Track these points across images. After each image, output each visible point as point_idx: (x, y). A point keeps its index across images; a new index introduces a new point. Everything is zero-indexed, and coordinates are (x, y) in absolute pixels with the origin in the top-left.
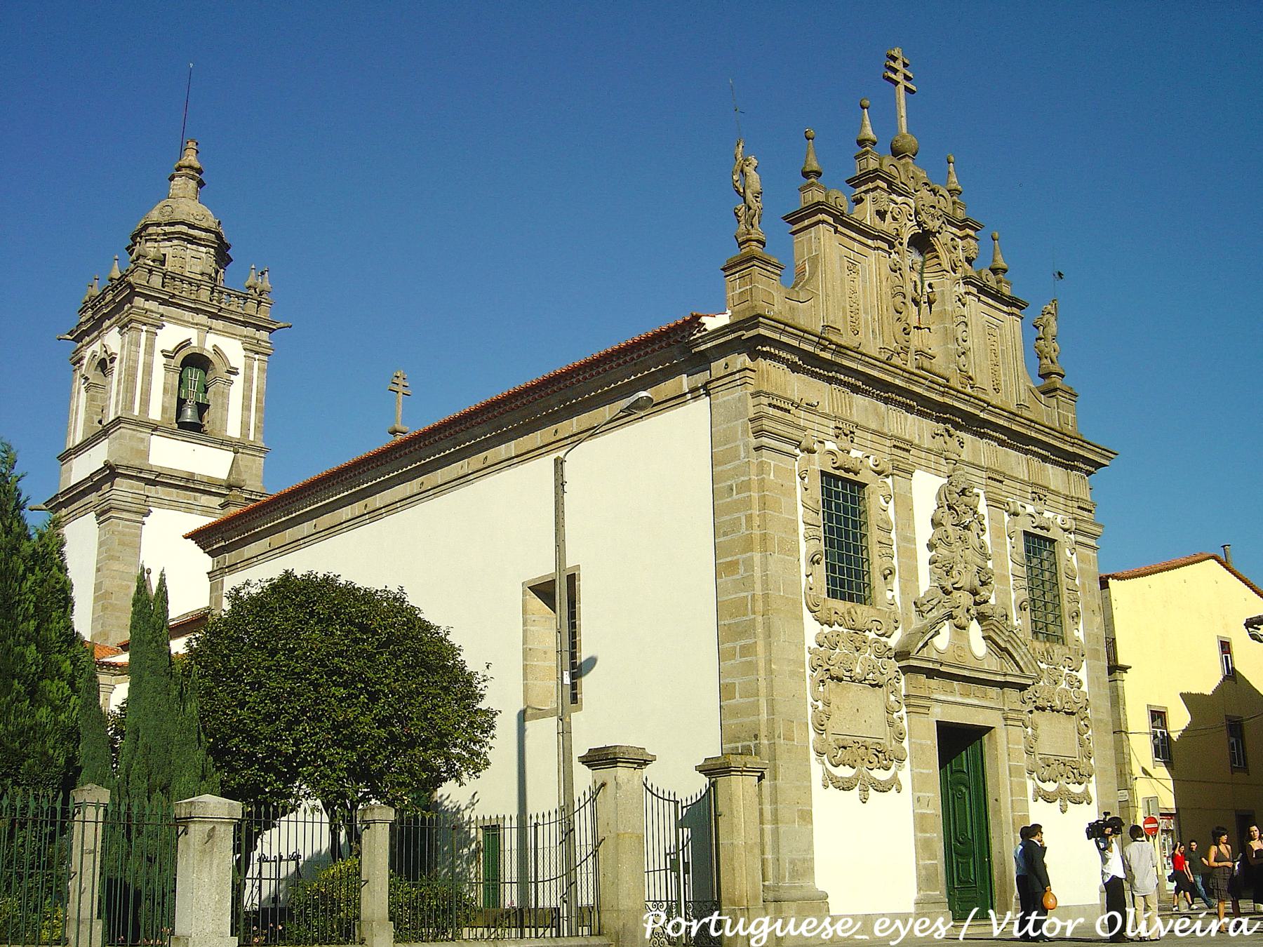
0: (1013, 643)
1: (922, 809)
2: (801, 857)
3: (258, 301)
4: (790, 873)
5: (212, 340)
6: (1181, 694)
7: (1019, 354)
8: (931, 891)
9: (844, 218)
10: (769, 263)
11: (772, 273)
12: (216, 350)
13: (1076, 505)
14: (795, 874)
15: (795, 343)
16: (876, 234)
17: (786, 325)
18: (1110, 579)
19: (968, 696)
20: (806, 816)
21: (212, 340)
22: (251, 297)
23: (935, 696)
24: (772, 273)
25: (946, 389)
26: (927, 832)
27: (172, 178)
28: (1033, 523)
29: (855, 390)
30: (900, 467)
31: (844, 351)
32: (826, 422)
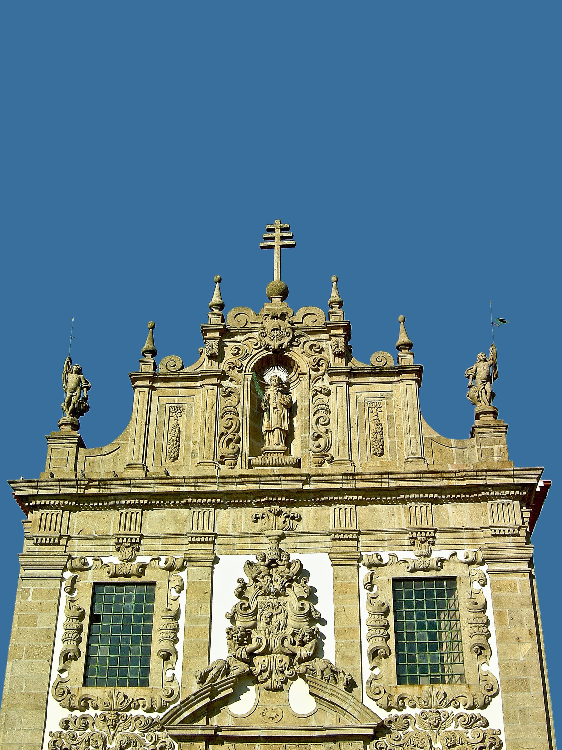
0: (337, 695)
6: (249, 690)
7: (411, 413)
9: (159, 376)
10: (63, 438)
11: (67, 443)
13: (489, 534)
15: (56, 491)
16: (200, 375)
18: (305, 597)
24: (67, 443)
25: (243, 479)
28: (408, 568)
29: (217, 506)
30: (192, 559)
31: (109, 482)
32: (105, 542)
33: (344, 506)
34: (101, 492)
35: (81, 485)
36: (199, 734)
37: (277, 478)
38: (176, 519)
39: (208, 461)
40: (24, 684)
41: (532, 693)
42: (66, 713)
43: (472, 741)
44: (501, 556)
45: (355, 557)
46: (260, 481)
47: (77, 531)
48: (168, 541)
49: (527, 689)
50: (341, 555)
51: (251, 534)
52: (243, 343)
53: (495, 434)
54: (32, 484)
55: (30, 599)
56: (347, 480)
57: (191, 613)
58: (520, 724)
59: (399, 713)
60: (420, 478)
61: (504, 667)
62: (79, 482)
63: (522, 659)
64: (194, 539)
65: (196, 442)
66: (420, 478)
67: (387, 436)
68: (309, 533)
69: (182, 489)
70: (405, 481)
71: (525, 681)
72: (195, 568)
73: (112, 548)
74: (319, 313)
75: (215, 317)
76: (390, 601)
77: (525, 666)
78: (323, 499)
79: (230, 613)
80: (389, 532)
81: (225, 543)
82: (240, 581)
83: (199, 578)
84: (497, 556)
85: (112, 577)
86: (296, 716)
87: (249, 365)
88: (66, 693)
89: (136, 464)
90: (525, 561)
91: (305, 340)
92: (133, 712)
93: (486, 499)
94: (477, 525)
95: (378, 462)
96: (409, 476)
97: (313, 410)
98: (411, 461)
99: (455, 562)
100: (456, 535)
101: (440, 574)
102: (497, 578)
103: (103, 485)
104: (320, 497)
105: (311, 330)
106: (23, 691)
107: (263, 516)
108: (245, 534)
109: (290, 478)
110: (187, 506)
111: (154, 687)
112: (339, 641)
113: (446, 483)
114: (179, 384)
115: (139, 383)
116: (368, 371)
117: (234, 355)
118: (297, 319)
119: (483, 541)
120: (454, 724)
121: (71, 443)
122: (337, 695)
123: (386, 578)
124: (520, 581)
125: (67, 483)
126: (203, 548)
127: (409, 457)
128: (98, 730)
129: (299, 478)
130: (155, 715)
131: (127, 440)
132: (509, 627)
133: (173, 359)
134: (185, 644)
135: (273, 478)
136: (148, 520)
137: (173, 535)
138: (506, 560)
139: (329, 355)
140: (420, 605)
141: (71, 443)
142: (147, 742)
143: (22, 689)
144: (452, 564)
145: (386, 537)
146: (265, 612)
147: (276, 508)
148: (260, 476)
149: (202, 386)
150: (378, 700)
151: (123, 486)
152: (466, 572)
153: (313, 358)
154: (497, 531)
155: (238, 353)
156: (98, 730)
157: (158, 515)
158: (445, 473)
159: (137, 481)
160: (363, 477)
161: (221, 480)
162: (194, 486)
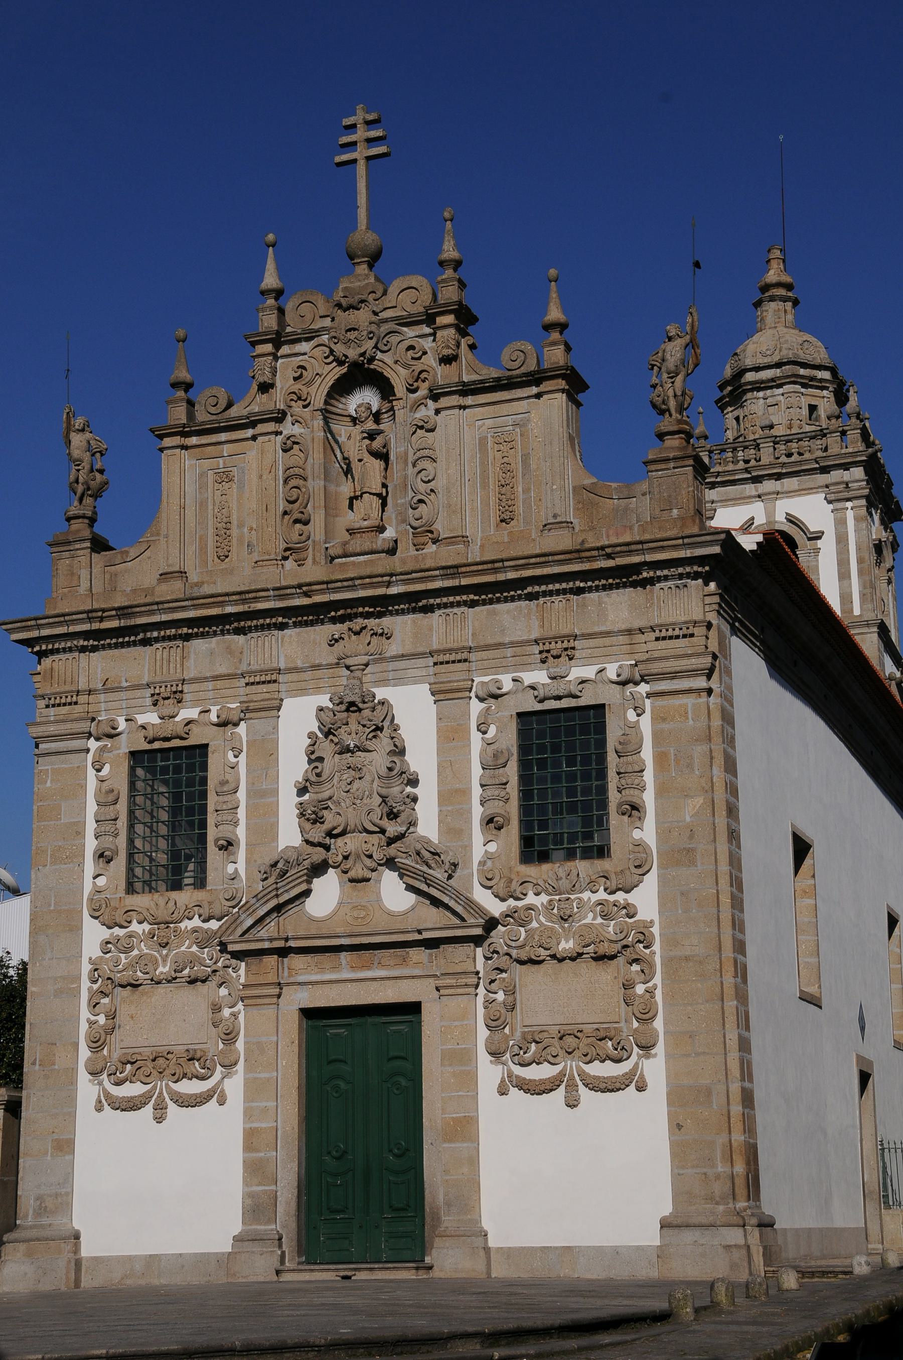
1: (252, 1122)
2: (54, 1191)
3: (840, 432)
4: (34, 1210)
5: (783, 508)
8: (261, 1224)
12: (791, 520)
14: (42, 1210)
17: (36, 619)
19: (369, 968)
20: (65, 1146)
21: (783, 508)
22: (828, 431)
23: (301, 979)
26: (258, 1151)
27: (758, 304)
30: (250, 708)
31: (130, 610)
32: (138, 693)
33: (451, 610)
34: (122, 625)
35: (93, 618)
36: (266, 947)
37: (350, 583)
38: (229, 651)
39: (267, 557)
40: (53, 899)
41: (699, 867)
42: (105, 933)
43: (614, 938)
44: (665, 670)
45: (465, 686)
46: (328, 589)
47: (101, 680)
48: (219, 684)
49: (692, 863)
50: (446, 685)
51: (327, 665)
52: (310, 355)
53: (676, 470)
54: (29, 623)
55: (49, 784)
56: (447, 575)
57: (253, 784)
58: (680, 912)
59: (520, 904)
60: (549, 562)
61: (663, 834)
62: (90, 615)
63: (688, 819)
64: (252, 680)
65: (251, 529)
66: (549, 562)
67: (520, 489)
68: (403, 656)
69: (229, 609)
70: (529, 569)
71: (690, 851)
72: (256, 721)
73: (149, 701)
74: (421, 286)
75: (268, 313)
76: (512, 746)
77: (691, 830)
78: (420, 604)
79: (301, 780)
80: (513, 644)
81: (294, 680)
82: (311, 735)
83: (262, 734)
84: (660, 671)
85: (150, 742)
86: (390, 914)
87: (318, 394)
88: (104, 906)
89: (172, 573)
90: (702, 675)
91: (400, 339)
92: (187, 925)
93: (651, 581)
94: (637, 624)
95: (506, 532)
96: (533, 560)
97: (411, 459)
98: (550, 530)
99: (603, 682)
100: (607, 641)
101: (582, 702)
102: (661, 702)
103: (122, 615)
104: (417, 601)
105: (408, 320)
106: (52, 908)
107: (343, 635)
108: (319, 666)
109: (368, 580)
110: (239, 631)
111: (214, 888)
112: (444, 808)
113: (586, 566)
114: (223, 437)
115: (167, 442)
116: (491, 384)
117: (295, 379)
118: (390, 301)
119: (644, 648)
120: (591, 915)
121: (82, 549)
122: (435, 885)
123: (507, 713)
124: (694, 705)
125: (74, 617)
126: (265, 690)
127: (549, 521)
128: (148, 951)
129: (380, 579)
130: (214, 925)
131: (158, 534)
132: (674, 775)
133: (214, 392)
134: (248, 828)
135: (345, 584)
136: (192, 656)
137: (225, 676)
138: (674, 675)
139: (430, 360)
140: (556, 748)
141: (82, 549)
142: (208, 961)
143: (50, 905)
144: (600, 685)
145: (509, 652)
146: (345, 776)
147: (359, 622)
148: (327, 583)
149: (254, 438)
150: (492, 887)
151: (148, 613)
152: (618, 696)
153: (411, 370)
154: (664, 630)
155: (301, 376)
156: (148, 951)
157: (206, 648)
158: (584, 551)
159: (166, 606)
160: (468, 569)
161: (277, 593)
162: (243, 604)
